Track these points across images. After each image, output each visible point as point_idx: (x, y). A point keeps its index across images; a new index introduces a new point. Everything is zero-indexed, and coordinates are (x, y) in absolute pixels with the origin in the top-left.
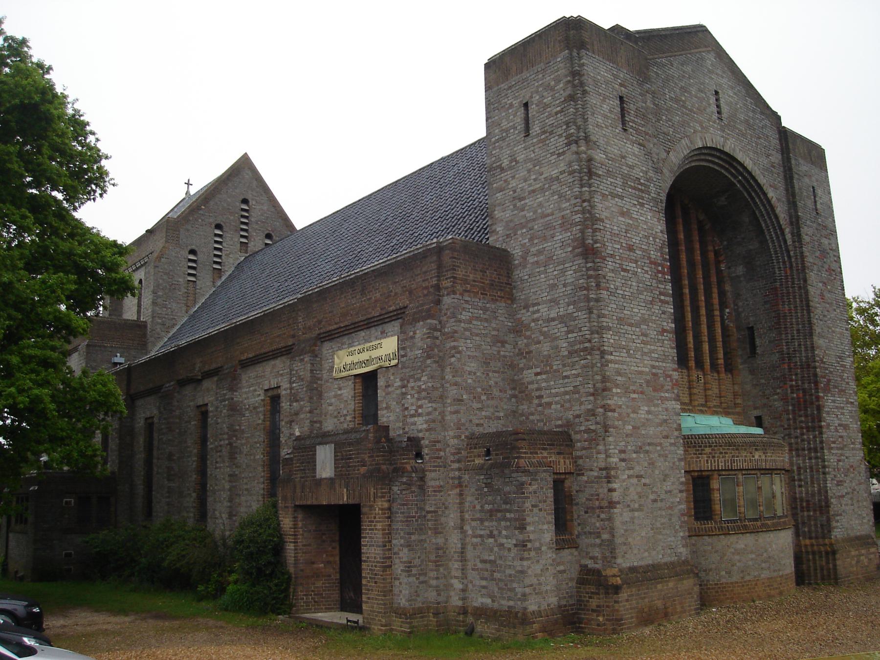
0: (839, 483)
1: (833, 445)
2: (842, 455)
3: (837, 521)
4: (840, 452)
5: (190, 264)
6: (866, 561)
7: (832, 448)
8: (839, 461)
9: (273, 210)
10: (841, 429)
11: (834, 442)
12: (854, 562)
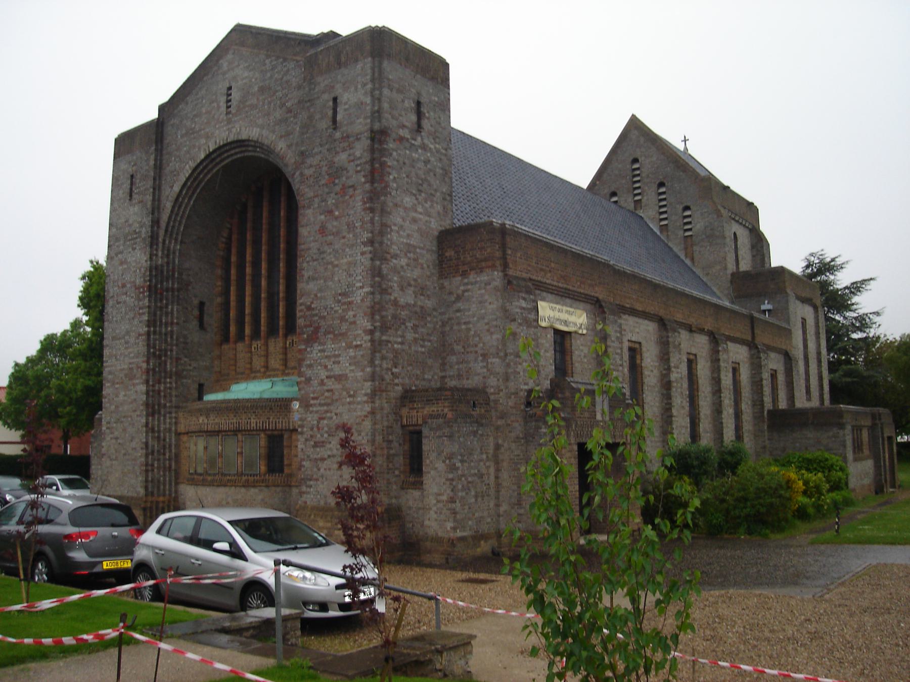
1: (312, 402)
2: (327, 412)
4: (325, 408)
10: (330, 384)
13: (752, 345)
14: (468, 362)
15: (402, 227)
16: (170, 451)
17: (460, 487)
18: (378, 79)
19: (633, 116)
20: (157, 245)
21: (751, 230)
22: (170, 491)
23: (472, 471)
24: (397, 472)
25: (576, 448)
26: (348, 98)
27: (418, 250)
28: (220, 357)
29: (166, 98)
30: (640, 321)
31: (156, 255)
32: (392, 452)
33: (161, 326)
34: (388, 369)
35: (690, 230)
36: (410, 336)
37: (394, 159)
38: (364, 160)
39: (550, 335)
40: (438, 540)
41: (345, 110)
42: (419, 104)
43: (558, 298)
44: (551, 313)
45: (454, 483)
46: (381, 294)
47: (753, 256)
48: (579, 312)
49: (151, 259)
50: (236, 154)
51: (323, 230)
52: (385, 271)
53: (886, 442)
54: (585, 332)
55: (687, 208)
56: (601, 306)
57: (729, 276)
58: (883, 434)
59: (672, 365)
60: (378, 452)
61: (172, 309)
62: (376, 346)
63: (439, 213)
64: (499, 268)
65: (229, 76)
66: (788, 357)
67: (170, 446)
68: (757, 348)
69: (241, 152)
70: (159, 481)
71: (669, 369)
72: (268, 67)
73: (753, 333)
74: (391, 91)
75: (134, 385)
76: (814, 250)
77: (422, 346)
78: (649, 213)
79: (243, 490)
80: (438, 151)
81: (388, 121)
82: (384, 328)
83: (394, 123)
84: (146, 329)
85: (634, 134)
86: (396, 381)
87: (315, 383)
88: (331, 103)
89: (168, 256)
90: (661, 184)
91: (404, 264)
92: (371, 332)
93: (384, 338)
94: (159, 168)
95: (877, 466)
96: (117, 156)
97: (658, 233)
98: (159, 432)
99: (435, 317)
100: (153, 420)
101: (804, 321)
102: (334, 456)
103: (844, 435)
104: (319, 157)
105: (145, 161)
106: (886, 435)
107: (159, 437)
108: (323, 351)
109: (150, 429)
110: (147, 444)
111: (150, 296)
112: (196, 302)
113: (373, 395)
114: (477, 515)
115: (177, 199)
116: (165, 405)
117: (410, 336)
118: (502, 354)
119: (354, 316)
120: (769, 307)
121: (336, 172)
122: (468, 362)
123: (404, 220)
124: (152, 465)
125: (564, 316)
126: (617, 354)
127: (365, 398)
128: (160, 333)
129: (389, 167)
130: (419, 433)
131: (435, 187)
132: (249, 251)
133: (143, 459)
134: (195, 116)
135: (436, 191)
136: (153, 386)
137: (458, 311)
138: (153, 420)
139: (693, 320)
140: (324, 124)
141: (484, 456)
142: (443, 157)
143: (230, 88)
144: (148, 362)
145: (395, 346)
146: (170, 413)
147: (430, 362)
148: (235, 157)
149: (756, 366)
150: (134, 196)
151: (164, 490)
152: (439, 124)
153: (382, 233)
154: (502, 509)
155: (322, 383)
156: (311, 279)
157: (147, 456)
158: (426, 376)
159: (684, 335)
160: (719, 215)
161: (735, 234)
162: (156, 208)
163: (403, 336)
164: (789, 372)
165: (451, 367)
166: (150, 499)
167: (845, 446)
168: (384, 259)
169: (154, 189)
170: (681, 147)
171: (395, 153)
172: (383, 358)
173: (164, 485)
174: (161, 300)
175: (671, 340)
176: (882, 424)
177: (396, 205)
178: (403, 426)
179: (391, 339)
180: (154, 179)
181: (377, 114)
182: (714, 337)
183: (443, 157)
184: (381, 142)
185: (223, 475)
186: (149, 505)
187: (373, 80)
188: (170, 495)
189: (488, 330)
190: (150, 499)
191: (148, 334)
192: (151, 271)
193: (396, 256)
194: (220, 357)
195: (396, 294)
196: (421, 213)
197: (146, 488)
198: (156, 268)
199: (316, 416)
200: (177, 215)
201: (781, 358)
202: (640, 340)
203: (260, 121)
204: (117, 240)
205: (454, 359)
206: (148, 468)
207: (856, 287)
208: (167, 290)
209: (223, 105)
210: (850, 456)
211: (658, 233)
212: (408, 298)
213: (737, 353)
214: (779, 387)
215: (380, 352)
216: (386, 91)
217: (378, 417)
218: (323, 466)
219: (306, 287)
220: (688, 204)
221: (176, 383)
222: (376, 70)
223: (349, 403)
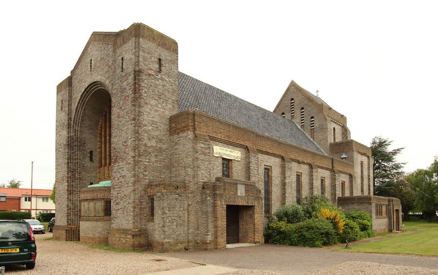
0: (117, 204)
1: (116, 187)
2: (120, 190)
3: (115, 221)
4: (119, 189)
5: (313, 122)
6: (124, 241)
7: (115, 188)
8: (118, 193)
9: (303, 97)
10: (121, 178)
11: (116, 185)
12: (117, 240)
13: (332, 170)
14: (179, 171)
15: (149, 113)
16: (77, 208)
17: (168, 221)
18: (137, 47)
20: (71, 128)
21: (342, 127)
22: (77, 223)
23: (175, 215)
24: (145, 215)
25: (225, 206)
26: (127, 57)
27: (158, 124)
28: (100, 172)
29: (72, 68)
30: (271, 157)
31: (70, 132)
32: (142, 206)
33: (73, 160)
34: (141, 172)
35: (313, 126)
36: (153, 159)
37: (146, 84)
38: (131, 84)
39: (220, 160)
40: (158, 243)
41: (126, 63)
42: (160, 60)
43: (225, 145)
44: (219, 150)
45: (164, 219)
46: (138, 141)
47: (343, 137)
48: (237, 152)
49: (68, 133)
50: (94, 89)
51: (118, 117)
52: (140, 132)
53: (395, 213)
54: (239, 160)
55: (313, 117)
56: (248, 150)
57: (329, 145)
58: (393, 208)
59: (286, 176)
60: (136, 206)
61: (77, 153)
62: (136, 163)
63: (170, 108)
64: (192, 130)
65: (91, 55)
66: (351, 176)
67: (77, 206)
68: (334, 171)
69: (96, 88)
70: (73, 219)
71: (285, 178)
72: (103, 49)
74: (144, 52)
75: (64, 183)
76: (377, 136)
77: (160, 164)
78: (297, 120)
79: (95, 222)
80: (170, 82)
81: (142, 66)
82: (140, 155)
84: (67, 161)
85: (292, 88)
86: (146, 178)
87: (116, 179)
88: (121, 61)
89: (75, 132)
90: (302, 108)
91: (150, 129)
92: (134, 157)
93: (139, 159)
94: (70, 96)
95: (390, 222)
96: (58, 93)
98: (73, 201)
99: (167, 152)
100: (70, 196)
101: (362, 163)
102: (122, 208)
103: (371, 208)
104: (117, 85)
105: (65, 93)
106: (395, 209)
107: (72, 203)
108: (118, 166)
109: (69, 200)
110: (68, 206)
111: (68, 148)
112: (89, 151)
113: (134, 183)
114: (177, 233)
115: (77, 109)
116: (75, 190)
117: (153, 159)
118: (192, 167)
119: (128, 151)
120: (345, 156)
121: (123, 90)
122: (179, 171)
123: (151, 110)
124: (70, 214)
126: (255, 170)
127: (131, 185)
128: (73, 163)
129: (143, 86)
130: (153, 199)
131: (168, 97)
132: (108, 130)
133: (67, 211)
134: (81, 74)
135: (169, 98)
136: (70, 183)
137: (176, 149)
138: (70, 196)
139: (300, 159)
140: (119, 70)
141: (182, 209)
142: (173, 84)
143: (91, 60)
144: (68, 174)
145: (145, 163)
146: (77, 193)
147: (164, 171)
148: (99, 88)
149: (333, 179)
150: (63, 109)
151: (75, 223)
152: (171, 69)
153: (139, 116)
154: (190, 231)
155: (118, 179)
156: (115, 136)
157: (68, 210)
158: (162, 176)
159: (294, 164)
160: (326, 120)
161: (334, 128)
162: (69, 114)
163: (149, 159)
164: (351, 182)
165: (173, 173)
166: (69, 226)
167: (371, 212)
168: (139, 126)
169: (69, 105)
170: (315, 94)
171: (145, 82)
172: (139, 168)
173: (75, 221)
174: (73, 149)
175: (286, 165)
176: (393, 204)
177: (146, 103)
178: (148, 196)
179: (143, 160)
180: (69, 101)
181: (137, 63)
182: (311, 166)
183: (173, 84)
184: (139, 76)
185: (89, 217)
186: (68, 229)
187: (135, 48)
188: (77, 225)
189: (186, 157)
190: (69, 226)
191: (68, 163)
192: (68, 138)
193: (145, 125)
194: (100, 172)
195: (146, 141)
196: (160, 108)
197: (68, 222)
198: (70, 137)
199: (116, 192)
200: (77, 115)
201: (348, 177)
203: (101, 73)
204: (58, 127)
205: (174, 169)
206: (68, 215)
207: (395, 153)
208: (75, 146)
209: (89, 67)
210: (374, 216)
212: (153, 143)
213: (324, 173)
214: (346, 188)
215: (138, 166)
216: (141, 53)
217: (137, 192)
218: (119, 212)
219: (114, 140)
220: (313, 116)
221: (80, 182)
222: (137, 43)
223: (127, 187)
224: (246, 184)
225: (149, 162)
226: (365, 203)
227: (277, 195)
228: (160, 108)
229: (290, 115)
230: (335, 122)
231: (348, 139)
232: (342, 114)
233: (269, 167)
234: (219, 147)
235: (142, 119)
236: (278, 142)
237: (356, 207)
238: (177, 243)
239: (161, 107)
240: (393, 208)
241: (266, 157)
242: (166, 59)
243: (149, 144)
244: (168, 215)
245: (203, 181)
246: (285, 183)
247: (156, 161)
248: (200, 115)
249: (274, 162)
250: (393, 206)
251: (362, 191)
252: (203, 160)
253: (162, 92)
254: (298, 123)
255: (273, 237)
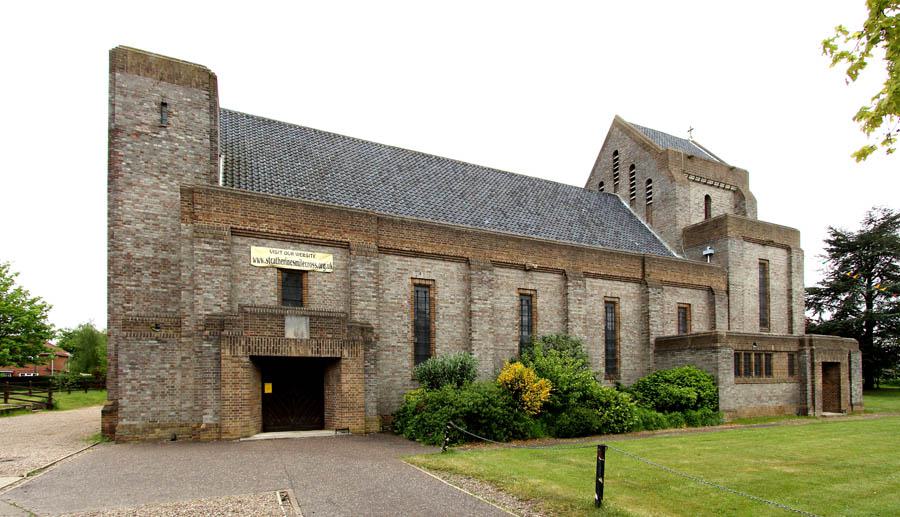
15: (138, 200)
19: (616, 116)
21: (734, 192)
36: (147, 280)
44: (261, 253)
58: (812, 359)
73: (644, 271)
74: (125, 96)
83: (129, 121)
97: (628, 206)
125: (282, 257)
158: (169, 310)
176: (812, 350)
179: (122, 283)
196: (164, 190)
202: (434, 278)
211: (628, 206)
212: (148, 252)
224: (311, 316)
225: (136, 286)
226: (706, 348)
227: (453, 338)
228: (164, 190)
229: (612, 185)
230: (710, 182)
231: (749, 216)
232: (731, 164)
233: (532, 293)
234: (269, 249)
235: (120, 213)
236: (452, 231)
237: (688, 359)
238: (152, 428)
239: (166, 187)
240: (812, 359)
241: (418, 262)
242: (180, 102)
243: (138, 255)
244: (129, 377)
245: (208, 313)
246: (470, 314)
247: (154, 282)
248: (208, 190)
249: (627, 294)
250: (812, 354)
251: (764, 322)
252: (210, 274)
253: (168, 162)
254: (624, 197)
255: (399, 425)
